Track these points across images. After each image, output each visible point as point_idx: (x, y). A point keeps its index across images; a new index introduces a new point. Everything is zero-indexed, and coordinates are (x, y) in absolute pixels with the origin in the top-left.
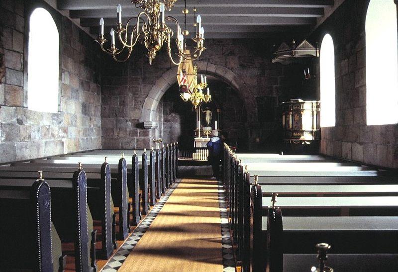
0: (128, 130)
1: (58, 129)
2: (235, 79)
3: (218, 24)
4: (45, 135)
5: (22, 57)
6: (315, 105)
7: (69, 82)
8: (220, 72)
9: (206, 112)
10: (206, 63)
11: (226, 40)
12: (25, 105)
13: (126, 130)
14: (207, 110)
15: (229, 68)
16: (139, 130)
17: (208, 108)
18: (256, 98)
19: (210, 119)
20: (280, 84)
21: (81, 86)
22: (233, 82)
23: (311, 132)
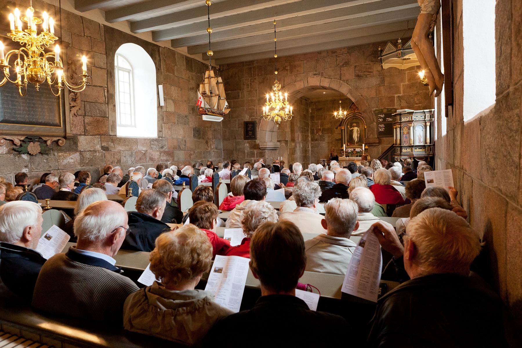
0: (246, 151)
1: (158, 153)
2: (350, 92)
3: (349, 28)
4: (140, 159)
5: (106, 91)
6: (428, 115)
7: (173, 108)
8: (334, 86)
9: (353, 130)
10: (320, 77)
11: (340, 49)
12: (111, 133)
13: (244, 152)
14: (354, 127)
15: (344, 81)
16: (255, 151)
17: (355, 124)
18: (374, 111)
19: (357, 137)
20: (404, 92)
21: (191, 112)
22: (349, 96)
23: (424, 147)
